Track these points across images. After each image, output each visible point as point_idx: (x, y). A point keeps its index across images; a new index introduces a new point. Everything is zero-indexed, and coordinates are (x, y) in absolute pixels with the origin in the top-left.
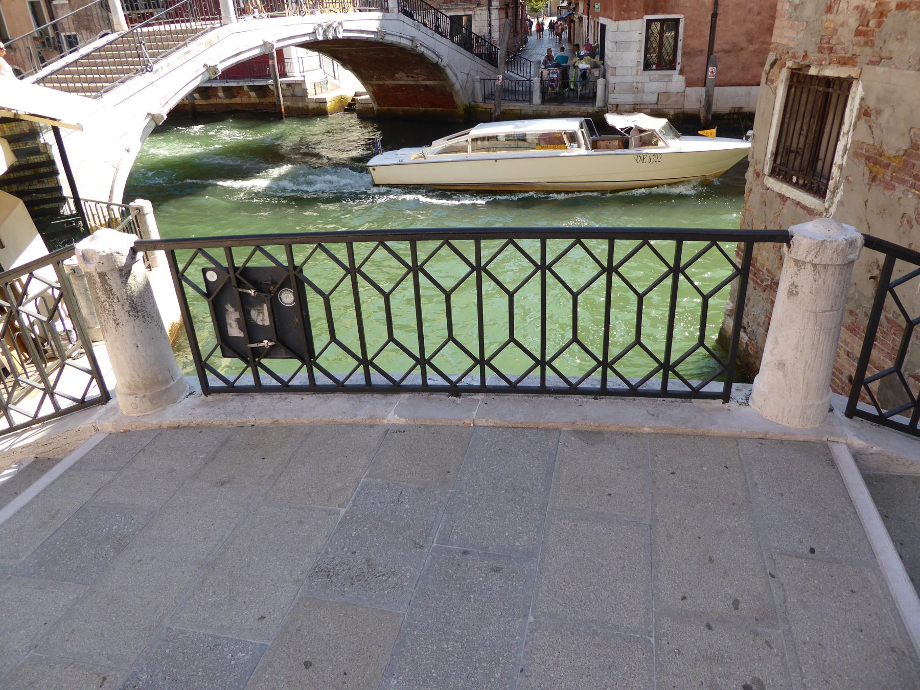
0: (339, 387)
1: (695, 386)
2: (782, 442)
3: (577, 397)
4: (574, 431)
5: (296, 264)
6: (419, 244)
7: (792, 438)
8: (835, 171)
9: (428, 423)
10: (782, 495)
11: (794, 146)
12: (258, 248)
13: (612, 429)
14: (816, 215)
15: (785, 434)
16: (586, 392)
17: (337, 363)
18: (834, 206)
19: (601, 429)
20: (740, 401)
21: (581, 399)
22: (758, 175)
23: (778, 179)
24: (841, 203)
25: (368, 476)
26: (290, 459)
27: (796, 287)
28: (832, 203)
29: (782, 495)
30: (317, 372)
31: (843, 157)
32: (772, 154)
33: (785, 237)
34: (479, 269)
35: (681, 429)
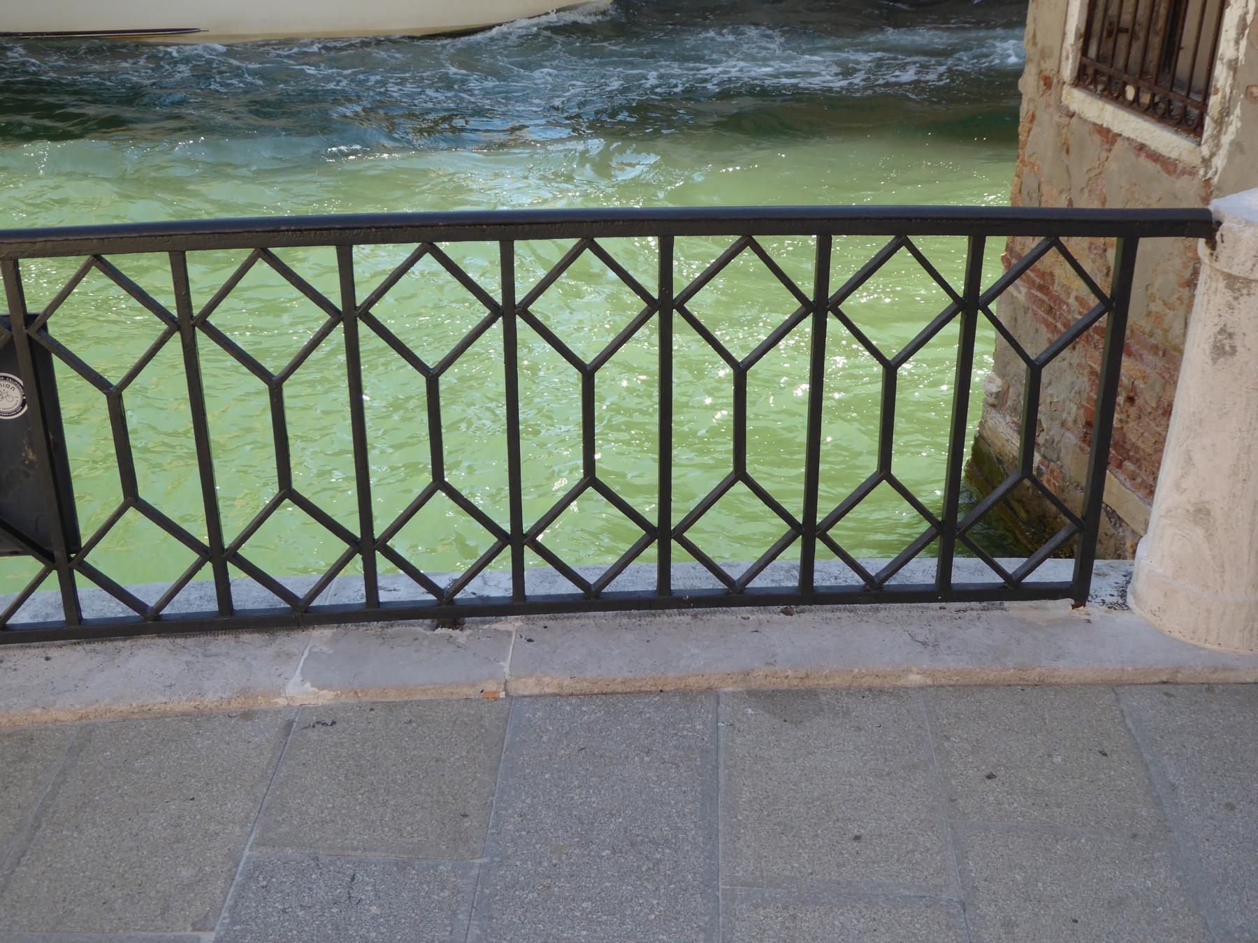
0: (149, 622)
1: (1010, 571)
2: (1210, 687)
3: (744, 611)
4: (752, 693)
5: (31, 309)
6: (360, 252)
7: (1232, 677)
8: (1221, 74)
9: (392, 697)
10: (1231, 807)
11: (1127, 18)
12: (98, 261)
13: (837, 681)
14: (1183, 173)
15: (1215, 670)
16: (340, 616)
17: (142, 561)
18: (1223, 152)
19: (809, 683)
20: (1109, 600)
21: (756, 615)
22: (1047, 82)
23: (1093, 93)
24: (1237, 146)
25: (260, 843)
26: (36, 818)
27: (1231, 336)
28: (1218, 146)
29: (1231, 807)
30: (84, 585)
31: (1237, 42)
32: (1078, 36)
33: (1201, 225)
34: (350, 315)
35: (991, 673)
